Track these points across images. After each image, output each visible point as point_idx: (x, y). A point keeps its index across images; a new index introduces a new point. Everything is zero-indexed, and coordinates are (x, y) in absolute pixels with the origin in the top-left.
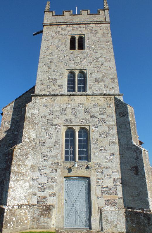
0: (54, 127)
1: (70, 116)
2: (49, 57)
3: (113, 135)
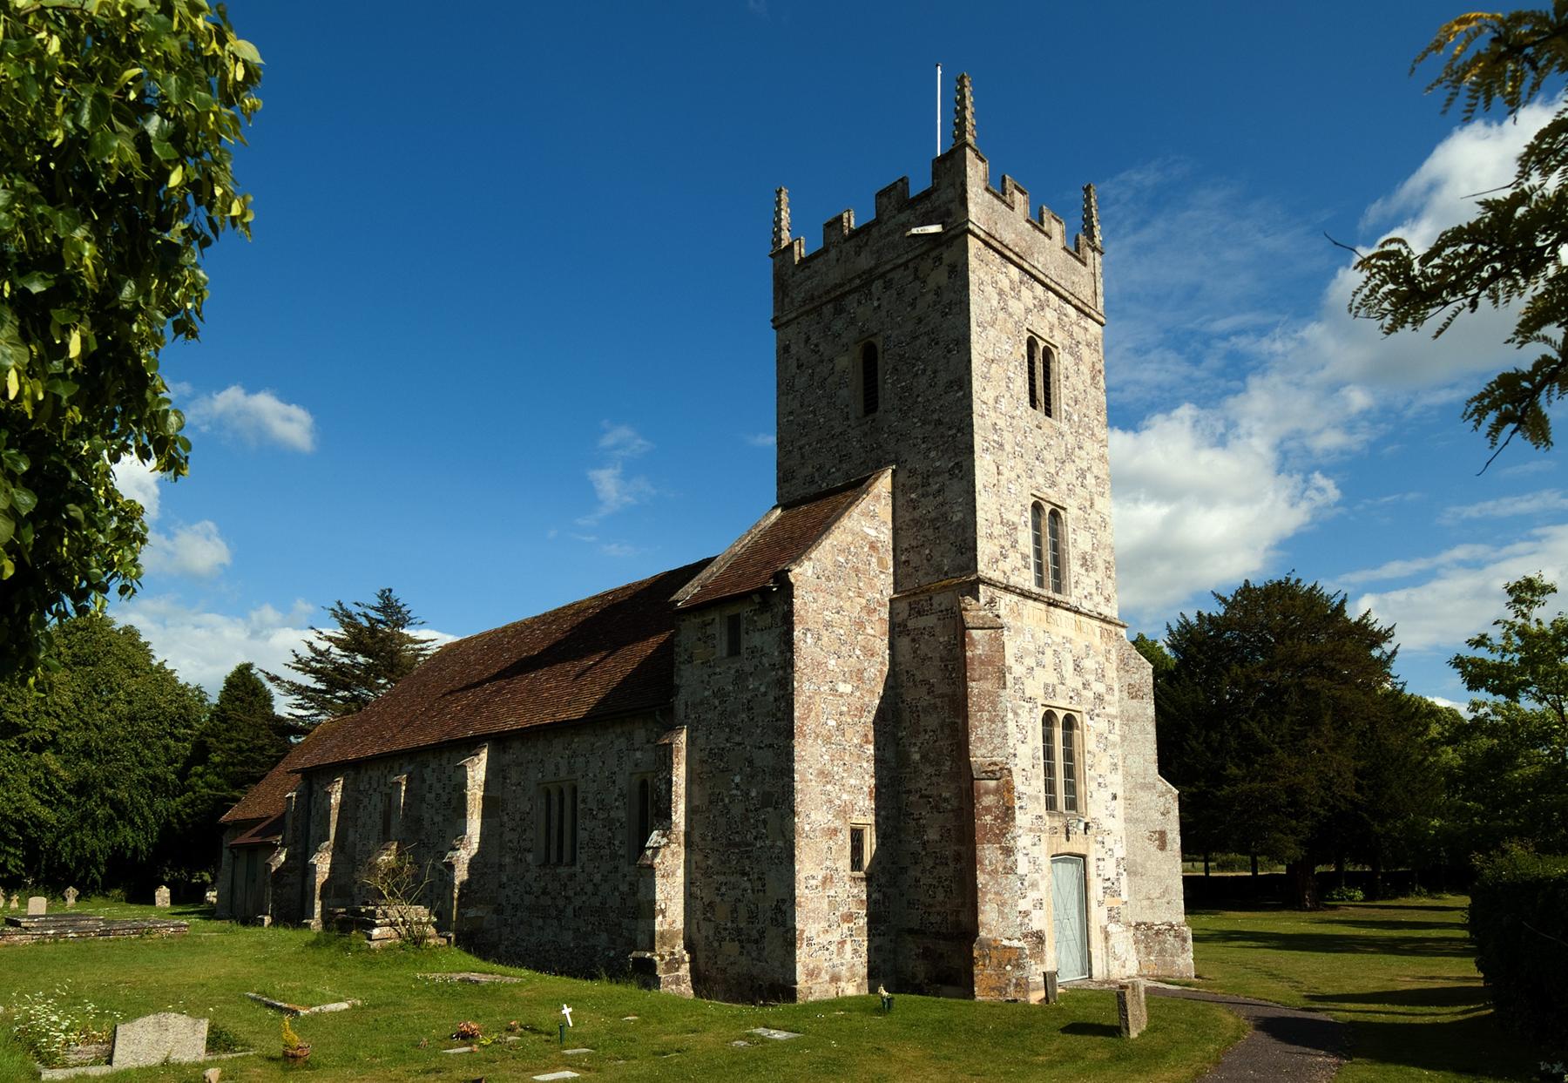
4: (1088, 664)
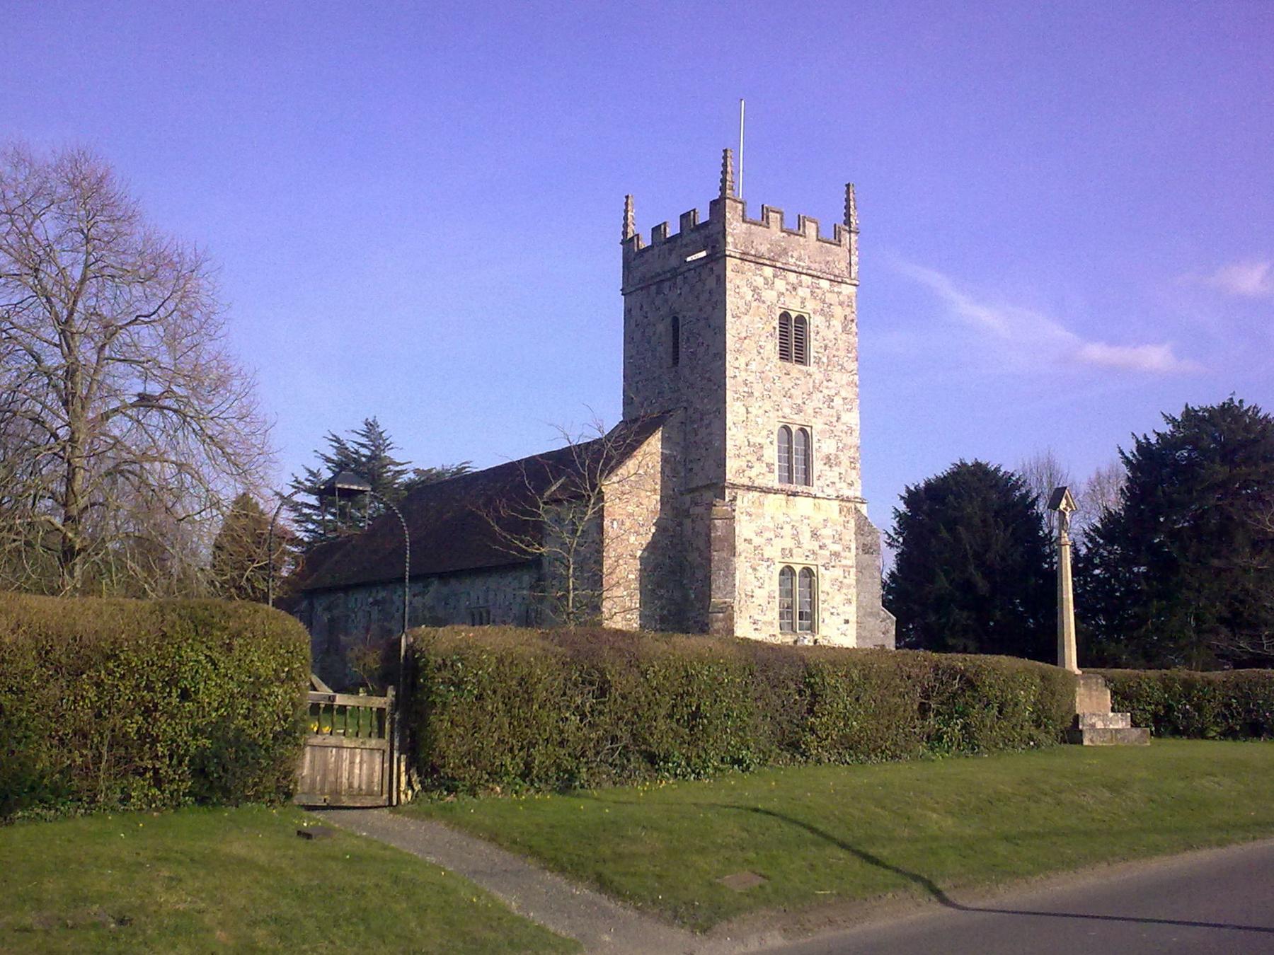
0: (765, 564)
3: (849, 587)
4: (826, 532)
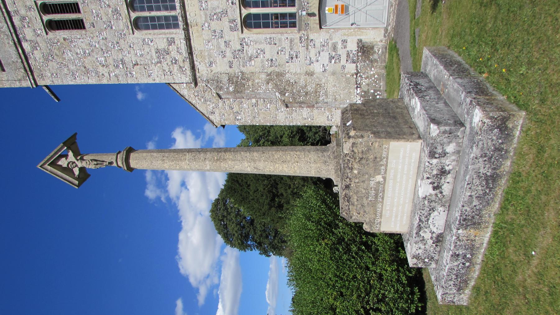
1: (225, 24)
2: (111, 68)
